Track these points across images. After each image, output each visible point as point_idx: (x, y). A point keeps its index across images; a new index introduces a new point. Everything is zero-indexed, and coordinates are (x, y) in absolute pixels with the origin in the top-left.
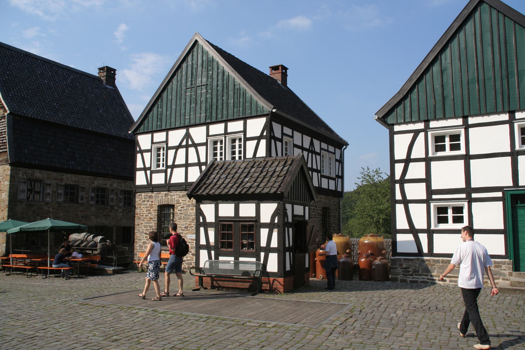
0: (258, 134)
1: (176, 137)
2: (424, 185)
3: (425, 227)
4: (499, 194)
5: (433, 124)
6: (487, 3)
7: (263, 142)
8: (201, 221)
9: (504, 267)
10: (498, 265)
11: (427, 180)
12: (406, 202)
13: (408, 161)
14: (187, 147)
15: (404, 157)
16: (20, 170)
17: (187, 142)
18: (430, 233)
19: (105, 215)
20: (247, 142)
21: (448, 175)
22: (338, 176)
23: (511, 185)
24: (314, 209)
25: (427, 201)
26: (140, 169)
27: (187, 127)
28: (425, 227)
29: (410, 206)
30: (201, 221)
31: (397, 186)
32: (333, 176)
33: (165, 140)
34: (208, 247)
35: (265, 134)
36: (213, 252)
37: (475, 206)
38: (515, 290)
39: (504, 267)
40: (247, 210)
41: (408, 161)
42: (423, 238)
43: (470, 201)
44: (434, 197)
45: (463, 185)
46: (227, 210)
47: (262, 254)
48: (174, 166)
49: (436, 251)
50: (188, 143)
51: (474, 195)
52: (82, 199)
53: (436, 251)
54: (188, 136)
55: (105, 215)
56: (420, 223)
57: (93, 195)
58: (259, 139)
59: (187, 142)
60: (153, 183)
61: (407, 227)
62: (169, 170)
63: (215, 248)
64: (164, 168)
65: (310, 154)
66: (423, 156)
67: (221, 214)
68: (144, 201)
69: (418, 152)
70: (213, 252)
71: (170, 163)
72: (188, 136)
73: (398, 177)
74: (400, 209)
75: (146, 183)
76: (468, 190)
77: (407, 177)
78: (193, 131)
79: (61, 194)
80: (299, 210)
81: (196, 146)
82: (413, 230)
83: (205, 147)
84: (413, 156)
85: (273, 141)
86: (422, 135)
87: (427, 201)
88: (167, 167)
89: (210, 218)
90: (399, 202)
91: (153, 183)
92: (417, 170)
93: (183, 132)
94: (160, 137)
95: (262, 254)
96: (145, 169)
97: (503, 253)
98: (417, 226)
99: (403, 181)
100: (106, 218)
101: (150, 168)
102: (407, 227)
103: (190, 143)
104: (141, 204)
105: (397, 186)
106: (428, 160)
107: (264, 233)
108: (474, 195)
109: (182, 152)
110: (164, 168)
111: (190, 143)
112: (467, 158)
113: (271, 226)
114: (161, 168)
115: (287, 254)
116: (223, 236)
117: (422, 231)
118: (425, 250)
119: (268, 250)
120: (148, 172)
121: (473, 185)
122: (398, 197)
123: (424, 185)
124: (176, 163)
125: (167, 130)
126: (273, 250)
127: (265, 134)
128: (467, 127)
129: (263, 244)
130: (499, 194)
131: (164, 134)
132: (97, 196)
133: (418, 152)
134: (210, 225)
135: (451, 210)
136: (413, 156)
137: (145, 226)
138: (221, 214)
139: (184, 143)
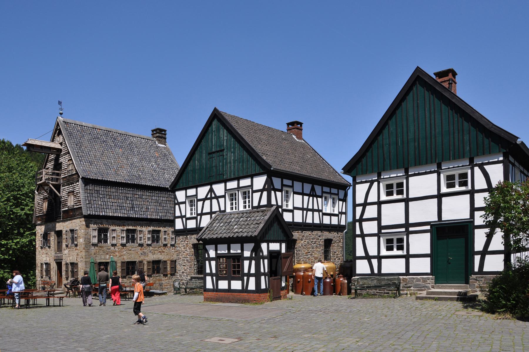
0: (261, 188)
1: (203, 192)
2: (376, 222)
3: (376, 254)
4: (428, 227)
5: (384, 176)
6: (44, 306)
7: (265, 193)
8: (207, 256)
9: (428, 281)
10: (424, 280)
11: (378, 219)
12: (363, 236)
13: (365, 205)
14: (211, 199)
15: (362, 201)
16: (91, 221)
17: (211, 195)
18: (380, 258)
19: (160, 252)
20: (254, 194)
21: (393, 214)
22: (341, 213)
23: (437, 220)
24: (316, 242)
25: (378, 235)
26: (178, 217)
27: (211, 184)
28: (376, 254)
29: (367, 239)
30: (207, 256)
31: (357, 224)
32: (336, 212)
33: (195, 194)
34: (264, 274)
35: (266, 187)
36: (214, 278)
37: (411, 236)
38: (430, 298)
39: (428, 281)
40: (235, 250)
41: (365, 205)
42: (375, 262)
43: (408, 233)
44: (383, 231)
45: (403, 222)
46: (223, 250)
47: (245, 278)
48: (202, 214)
49: (411, 271)
50: (212, 196)
51: (411, 229)
52: (140, 240)
53: (411, 271)
54: (211, 191)
55: (160, 252)
56: (373, 252)
57: (150, 236)
58: (262, 191)
59: (211, 195)
60: (188, 227)
61: (363, 254)
62: (199, 217)
63: (216, 275)
64: (196, 216)
65: (311, 198)
66: (376, 200)
67: (270, 249)
68: (182, 241)
69: (372, 198)
70: (214, 278)
71: (199, 212)
72: (211, 191)
73: (358, 217)
74: (359, 240)
75: (182, 228)
76: (407, 225)
77: (364, 217)
78: (215, 187)
79: (124, 237)
80: (275, 246)
81: (217, 198)
82: (368, 257)
83: (223, 199)
84: (369, 201)
85: (273, 192)
86: (376, 184)
87: (378, 235)
88: (198, 215)
89: (265, 253)
90: (358, 236)
91: (188, 227)
92: (371, 212)
93: (208, 188)
94: (191, 192)
95: (245, 278)
96: (181, 217)
97: (429, 271)
98: (371, 254)
99: (361, 220)
100: (161, 254)
101: (185, 216)
102: (363, 254)
103: (213, 196)
104: (180, 244)
105: (357, 224)
106: (379, 203)
107: (246, 263)
108: (411, 229)
109: (207, 202)
110: (196, 216)
111: (213, 196)
112: (407, 201)
113: (250, 259)
114: (194, 215)
115: (263, 278)
116: (239, 266)
117: (374, 257)
118: (376, 271)
119: (249, 275)
120: (184, 219)
121: (411, 221)
122: (358, 232)
123: (376, 222)
124: (204, 212)
125: (196, 187)
126: (252, 275)
127: (266, 187)
128: (407, 176)
129: (246, 271)
130: (428, 227)
131: (194, 190)
132: (153, 237)
133: (372, 198)
134: (213, 259)
135: (396, 239)
136: (369, 201)
137: (183, 260)
138: (270, 249)
139: (209, 196)
